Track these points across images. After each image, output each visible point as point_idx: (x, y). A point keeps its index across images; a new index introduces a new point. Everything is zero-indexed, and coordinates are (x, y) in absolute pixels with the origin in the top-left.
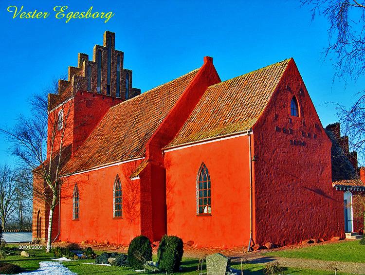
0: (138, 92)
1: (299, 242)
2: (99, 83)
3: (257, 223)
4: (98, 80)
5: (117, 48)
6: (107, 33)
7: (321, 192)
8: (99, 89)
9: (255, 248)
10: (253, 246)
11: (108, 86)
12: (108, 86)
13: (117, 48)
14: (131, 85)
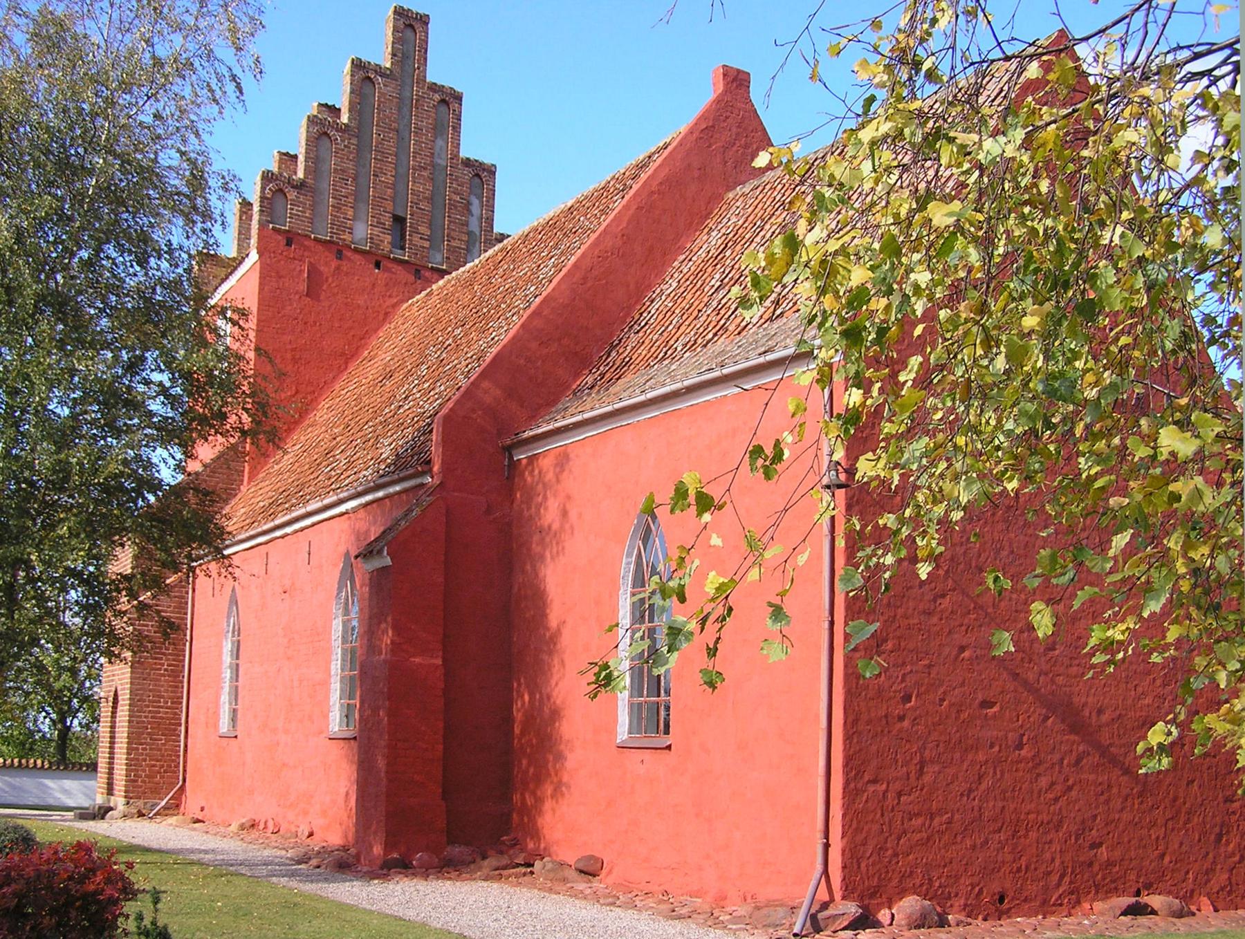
0: (502, 237)
1: (1078, 902)
2: (362, 206)
3: (850, 793)
4: (356, 194)
5: (435, 74)
6: (395, 12)
7: (534, 417)
8: (361, 232)
9: (835, 917)
10: (825, 906)
11: (399, 220)
12: (399, 220)
13: (435, 74)
14: (490, 221)
